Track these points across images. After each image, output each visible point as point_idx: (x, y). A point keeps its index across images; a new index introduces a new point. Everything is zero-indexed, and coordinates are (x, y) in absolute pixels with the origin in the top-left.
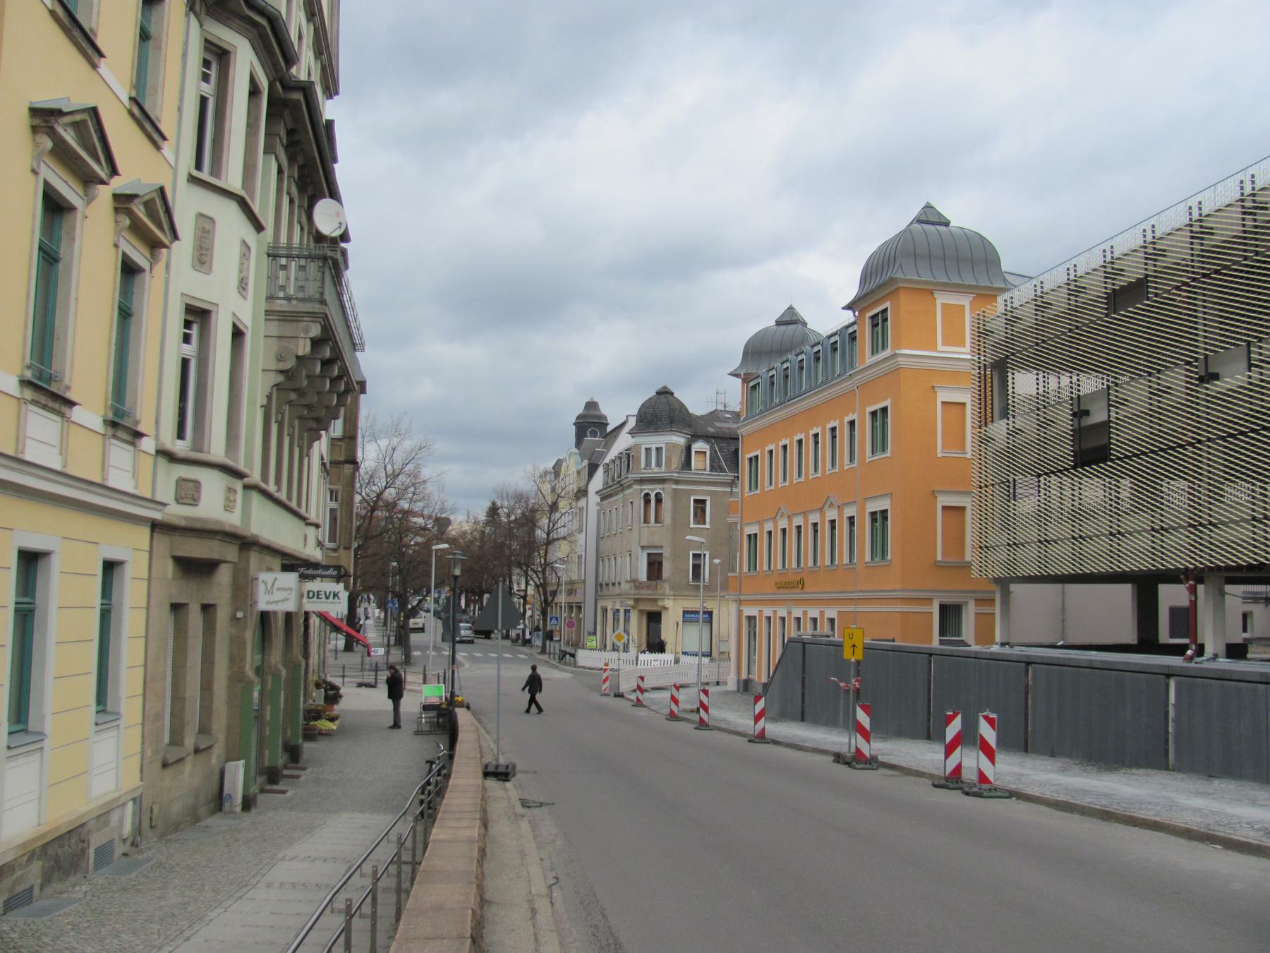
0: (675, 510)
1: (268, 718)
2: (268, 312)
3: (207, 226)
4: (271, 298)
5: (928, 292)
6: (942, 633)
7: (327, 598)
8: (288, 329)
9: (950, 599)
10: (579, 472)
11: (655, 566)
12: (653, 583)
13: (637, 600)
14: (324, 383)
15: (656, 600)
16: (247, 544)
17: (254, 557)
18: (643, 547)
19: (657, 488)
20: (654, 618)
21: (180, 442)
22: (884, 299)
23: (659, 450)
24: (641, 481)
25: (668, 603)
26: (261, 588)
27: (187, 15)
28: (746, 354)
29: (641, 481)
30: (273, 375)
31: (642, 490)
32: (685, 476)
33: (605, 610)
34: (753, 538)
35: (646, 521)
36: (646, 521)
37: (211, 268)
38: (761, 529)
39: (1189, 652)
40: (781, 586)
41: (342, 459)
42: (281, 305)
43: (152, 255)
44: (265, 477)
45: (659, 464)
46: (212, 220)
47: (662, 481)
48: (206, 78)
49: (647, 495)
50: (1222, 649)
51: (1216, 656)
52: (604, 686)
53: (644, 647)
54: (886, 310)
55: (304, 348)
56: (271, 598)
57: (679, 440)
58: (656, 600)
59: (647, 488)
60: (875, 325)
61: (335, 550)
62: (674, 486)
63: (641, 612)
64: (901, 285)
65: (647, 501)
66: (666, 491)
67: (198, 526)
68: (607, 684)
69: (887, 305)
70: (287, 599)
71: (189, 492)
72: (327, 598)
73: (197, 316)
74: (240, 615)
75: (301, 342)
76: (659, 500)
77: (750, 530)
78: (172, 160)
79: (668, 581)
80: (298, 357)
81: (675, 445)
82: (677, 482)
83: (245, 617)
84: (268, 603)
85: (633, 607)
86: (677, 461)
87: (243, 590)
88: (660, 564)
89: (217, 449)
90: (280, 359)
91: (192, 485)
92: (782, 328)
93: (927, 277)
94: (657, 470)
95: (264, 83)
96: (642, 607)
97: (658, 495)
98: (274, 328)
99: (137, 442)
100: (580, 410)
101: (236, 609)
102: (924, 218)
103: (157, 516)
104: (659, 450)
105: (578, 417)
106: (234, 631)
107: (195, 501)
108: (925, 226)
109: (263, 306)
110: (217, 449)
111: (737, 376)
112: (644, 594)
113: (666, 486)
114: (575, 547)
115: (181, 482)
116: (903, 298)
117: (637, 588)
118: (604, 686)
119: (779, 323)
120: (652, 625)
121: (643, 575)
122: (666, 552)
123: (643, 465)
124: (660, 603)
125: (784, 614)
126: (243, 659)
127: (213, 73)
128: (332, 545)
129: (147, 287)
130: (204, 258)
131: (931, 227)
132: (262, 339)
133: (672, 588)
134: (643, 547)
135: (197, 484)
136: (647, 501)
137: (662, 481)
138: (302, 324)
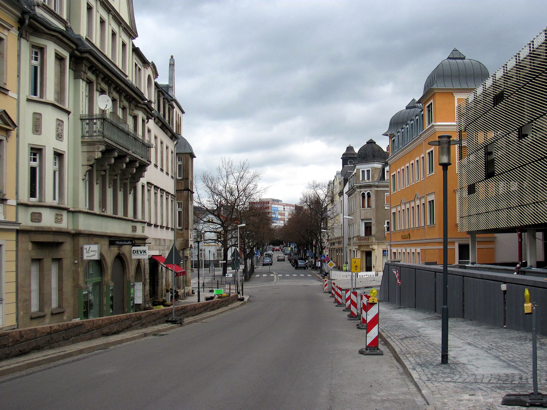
0: (377, 201)
1: (105, 303)
2: (82, 142)
3: (38, 117)
4: (83, 137)
5: (450, 93)
6: (460, 258)
7: (141, 253)
8: (91, 149)
9: (463, 242)
10: (340, 183)
11: (368, 228)
12: (367, 237)
13: (360, 246)
14: (123, 165)
15: (369, 246)
16: (76, 235)
17: (81, 240)
18: (362, 220)
19: (368, 190)
20: (369, 254)
21: (33, 199)
22: (428, 100)
23: (368, 171)
24: (360, 187)
25: (375, 247)
26: (85, 251)
27: (19, 40)
28: (391, 124)
29: (360, 187)
30: (86, 167)
31: (361, 192)
32: (381, 184)
33: (350, 251)
34: (394, 213)
35: (363, 207)
36: (363, 207)
37: (41, 132)
38: (397, 210)
39: (518, 265)
40: (404, 237)
41: (183, 189)
42: (87, 139)
43: (7, 134)
44: (91, 206)
45: (368, 178)
46: (40, 114)
47: (370, 186)
48: (36, 59)
49: (363, 194)
50: (534, 264)
51: (531, 267)
52: (325, 289)
53: (364, 269)
54: (431, 104)
55: (98, 155)
56: (89, 255)
57: (379, 166)
58: (369, 246)
59: (363, 190)
60: (429, 111)
61: (181, 230)
62: (376, 189)
63: (362, 251)
64: (436, 91)
65: (364, 197)
66: (372, 191)
67: (40, 230)
68: (327, 287)
69: (432, 101)
70: (94, 255)
71: (36, 217)
72: (141, 253)
73: (36, 152)
74: (76, 262)
75: (96, 153)
76: (369, 196)
77: (393, 210)
78: (16, 96)
79: (374, 236)
80: (96, 159)
81: (376, 168)
82: (377, 187)
83: (78, 262)
84: (87, 257)
85: (358, 249)
86: (376, 178)
87: (78, 252)
88: (371, 227)
89: (49, 200)
90: (88, 160)
91: (38, 215)
92: (408, 110)
93: (449, 86)
94: (367, 181)
95: (66, 54)
96: (362, 250)
97: (368, 194)
98: (85, 149)
99: (5, 202)
100: (344, 151)
101: (75, 260)
102: (451, 56)
103: (18, 228)
104: (368, 171)
105: (343, 155)
106: (74, 268)
107: (39, 220)
108: (458, 61)
109: (80, 140)
110: (49, 200)
111: (387, 135)
112: (363, 242)
113: (372, 189)
114: (344, 219)
115: (33, 214)
116: (437, 97)
117: (359, 240)
118: (325, 289)
119: (407, 108)
120: (368, 258)
121: (363, 234)
122: (373, 222)
123: (361, 179)
124: (370, 247)
125: (396, 251)
126: (78, 279)
127: (39, 57)
128: (180, 228)
129: (5, 146)
130: (37, 129)
131: (454, 61)
132: (80, 153)
133: (376, 239)
134: (362, 220)
135: (40, 214)
136: (364, 197)
137: (370, 186)
138: (97, 146)
